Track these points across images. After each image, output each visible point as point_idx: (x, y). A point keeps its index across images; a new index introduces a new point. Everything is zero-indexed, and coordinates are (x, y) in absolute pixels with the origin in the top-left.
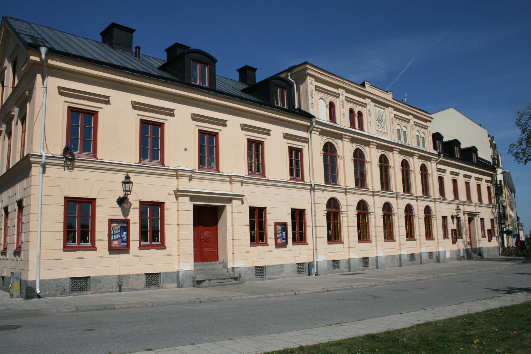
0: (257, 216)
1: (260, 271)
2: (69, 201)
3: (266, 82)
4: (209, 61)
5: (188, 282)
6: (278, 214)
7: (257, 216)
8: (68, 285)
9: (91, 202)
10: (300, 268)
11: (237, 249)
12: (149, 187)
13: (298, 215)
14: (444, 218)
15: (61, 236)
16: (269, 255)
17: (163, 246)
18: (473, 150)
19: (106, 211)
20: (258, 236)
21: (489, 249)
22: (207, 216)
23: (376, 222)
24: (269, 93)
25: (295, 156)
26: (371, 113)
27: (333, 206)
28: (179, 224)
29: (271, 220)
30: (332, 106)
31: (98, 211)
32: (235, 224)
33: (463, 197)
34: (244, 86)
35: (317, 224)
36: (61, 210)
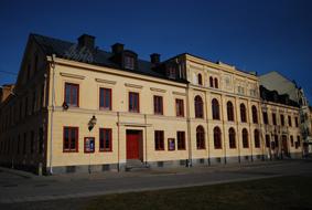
0: (159, 135)
1: (161, 163)
2: (66, 129)
3: (164, 64)
4: (133, 55)
5: (123, 169)
6: (170, 134)
7: (159, 135)
8: (65, 170)
9: (77, 129)
10: (182, 162)
11: (151, 155)
12: (105, 120)
13: (181, 135)
14: (267, 136)
15: (62, 145)
16: (167, 156)
17: (111, 151)
18: (286, 96)
19: (83, 133)
20: (159, 145)
21: (296, 154)
22: (134, 136)
23: (239, 140)
24: (169, 70)
25: (179, 102)
26: (222, 77)
27: (200, 131)
28: (119, 141)
29: (166, 137)
30: (200, 76)
31: (80, 133)
32: (149, 141)
33: (279, 123)
34: (154, 66)
35: (192, 139)
36: (62, 133)
